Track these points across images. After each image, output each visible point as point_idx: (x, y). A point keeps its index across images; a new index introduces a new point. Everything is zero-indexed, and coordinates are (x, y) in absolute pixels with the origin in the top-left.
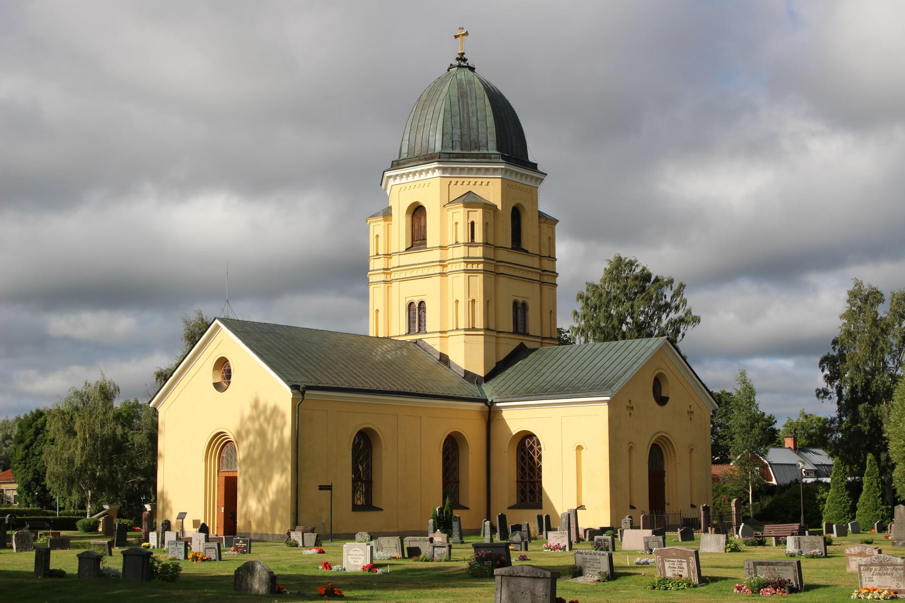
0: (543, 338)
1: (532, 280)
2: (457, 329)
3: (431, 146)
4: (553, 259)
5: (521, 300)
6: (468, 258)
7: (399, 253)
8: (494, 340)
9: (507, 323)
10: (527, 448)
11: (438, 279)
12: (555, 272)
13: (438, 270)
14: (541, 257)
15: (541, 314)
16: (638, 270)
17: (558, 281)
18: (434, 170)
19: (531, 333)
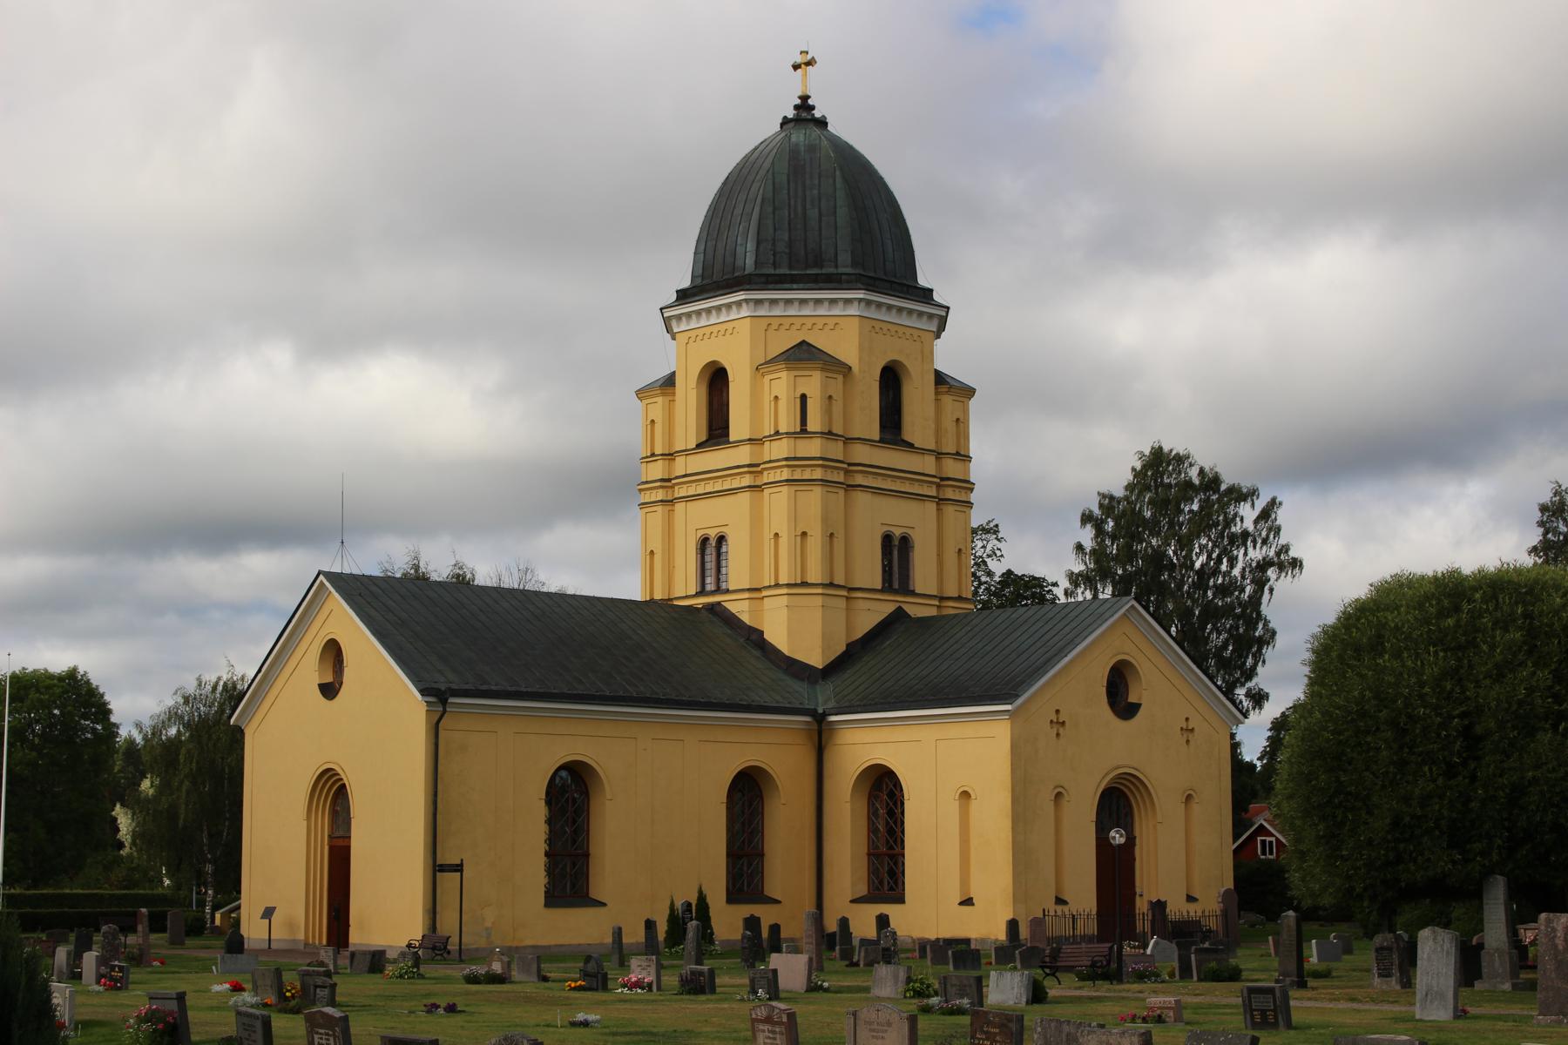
0: (942, 599)
2: (777, 585)
3: (739, 263)
4: (963, 457)
5: (898, 532)
6: (795, 459)
8: (842, 603)
9: (869, 571)
10: (883, 789)
12: (968, 482)
13: (746, 481)
14: (939, 455)
15: (940, 555)
16: (1193, 473)
18: (739, 304)
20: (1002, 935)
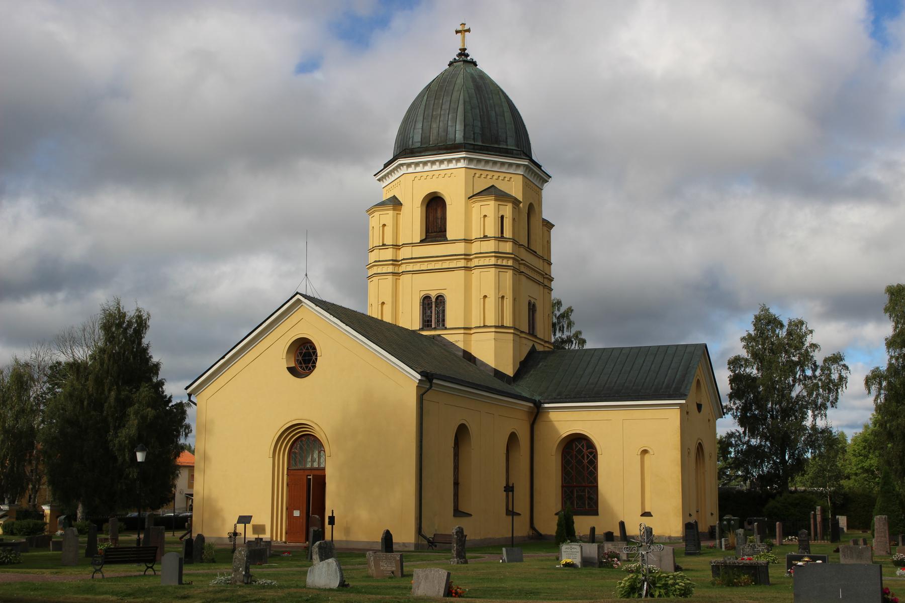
1: (538, 283)
2: (485, 326)
3: (451, 136)
7: (412, 244)
10: (579, 454)
11: (462, 273)
17: (553, 285)
18: (458, 160)
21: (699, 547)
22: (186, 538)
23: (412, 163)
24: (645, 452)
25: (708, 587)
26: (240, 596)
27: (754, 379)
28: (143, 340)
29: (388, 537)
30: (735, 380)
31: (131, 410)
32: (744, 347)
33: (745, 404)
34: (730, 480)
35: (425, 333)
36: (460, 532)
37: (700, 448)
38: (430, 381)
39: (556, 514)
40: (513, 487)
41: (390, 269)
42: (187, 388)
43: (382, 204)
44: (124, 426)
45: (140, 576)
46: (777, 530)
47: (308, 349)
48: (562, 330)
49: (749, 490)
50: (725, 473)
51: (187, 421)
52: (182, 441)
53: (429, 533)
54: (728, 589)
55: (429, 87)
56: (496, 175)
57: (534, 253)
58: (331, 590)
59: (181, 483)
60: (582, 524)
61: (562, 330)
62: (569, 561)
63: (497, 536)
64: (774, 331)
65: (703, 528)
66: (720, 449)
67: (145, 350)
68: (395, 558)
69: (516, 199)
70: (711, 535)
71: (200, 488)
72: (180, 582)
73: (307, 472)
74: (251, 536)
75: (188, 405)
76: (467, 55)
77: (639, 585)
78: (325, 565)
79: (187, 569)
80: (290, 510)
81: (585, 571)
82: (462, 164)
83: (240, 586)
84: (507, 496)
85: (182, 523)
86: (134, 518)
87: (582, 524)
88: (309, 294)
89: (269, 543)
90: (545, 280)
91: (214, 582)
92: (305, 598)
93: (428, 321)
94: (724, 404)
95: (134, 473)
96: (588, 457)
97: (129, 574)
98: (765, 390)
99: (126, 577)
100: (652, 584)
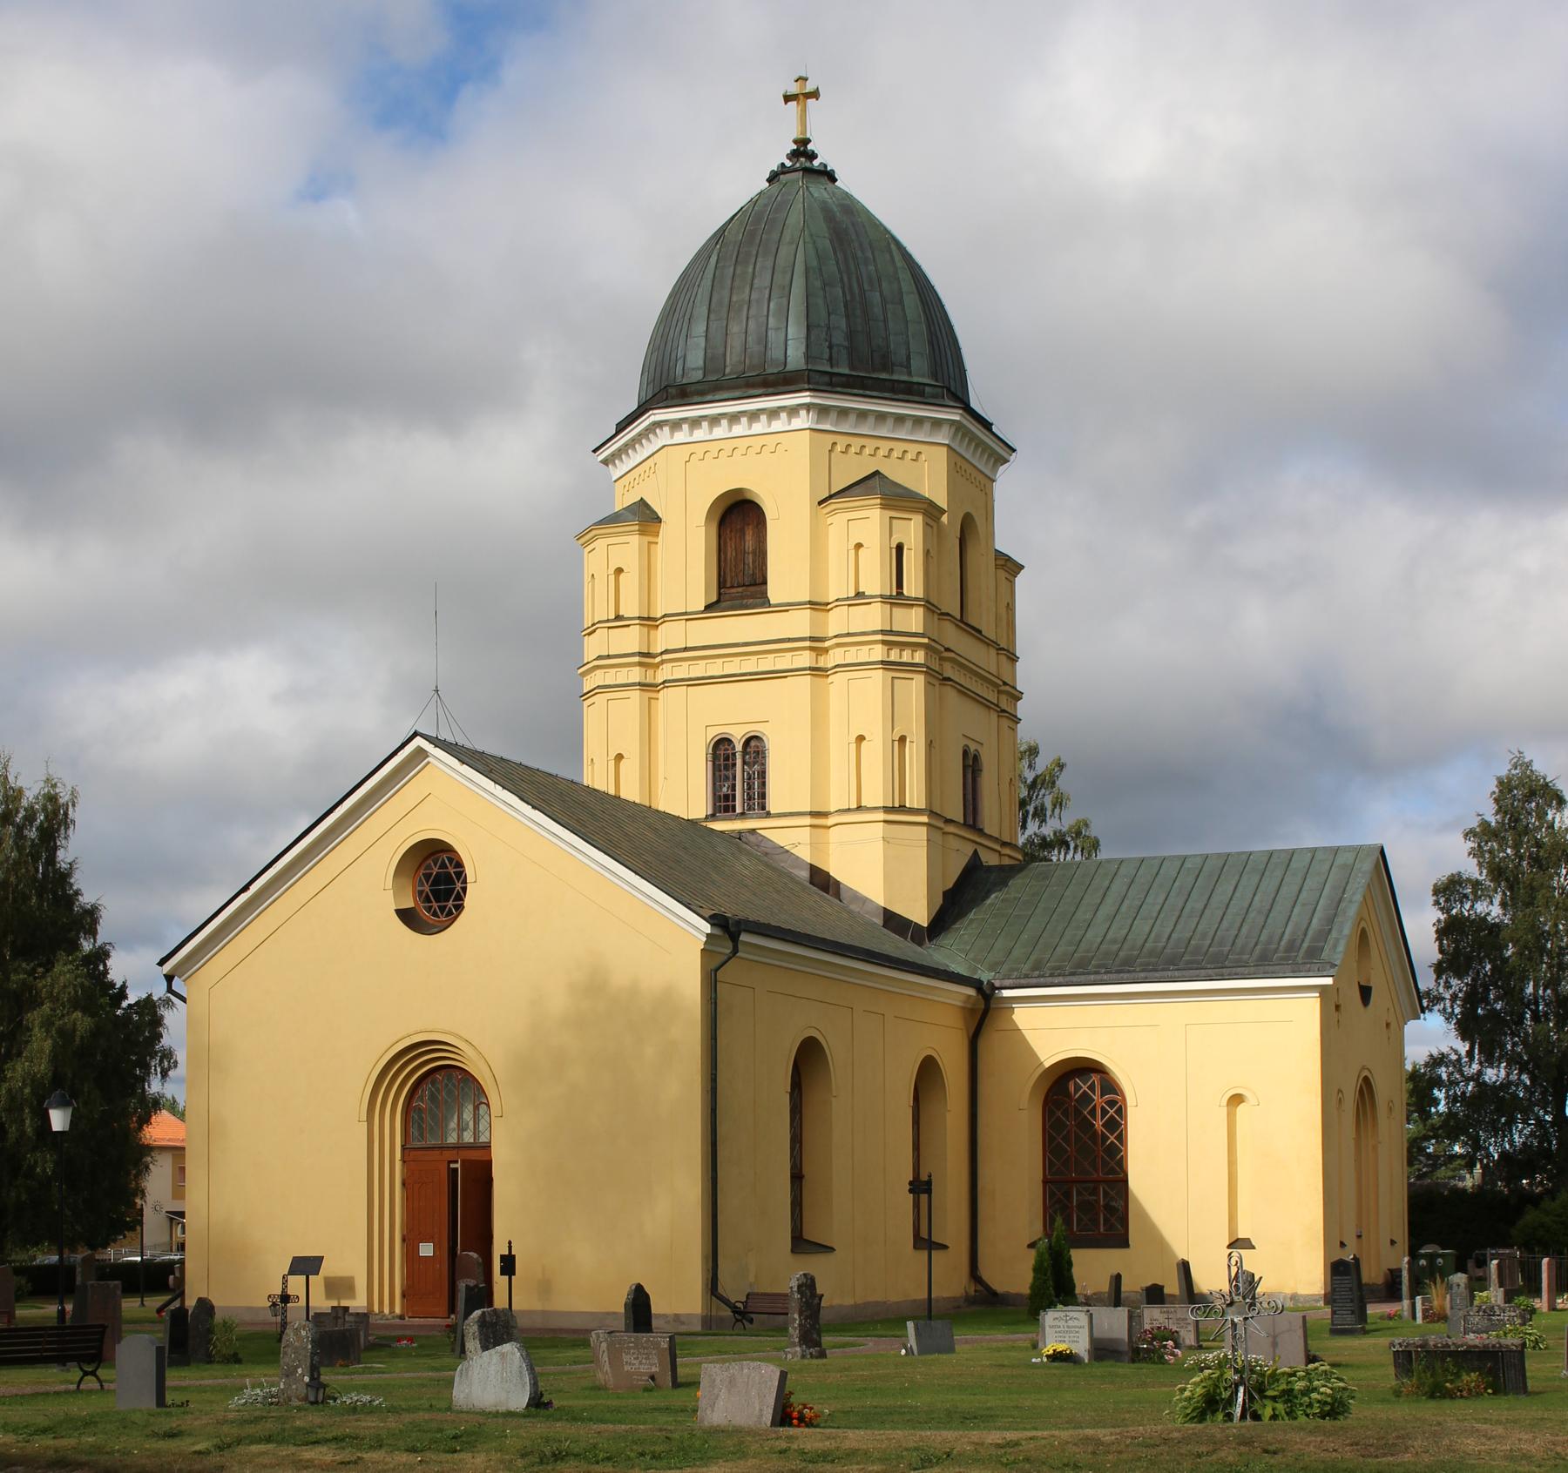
2: (859, 808)
3: (775, 353)
6: (891, 632)
10: (1081, 1110)
11: (806, 681)
13: (805, 659)
17: (1022, 709)
18: (793, 411)
19: (986, 831)
20: (1226, 1288)
21: (1362, 1317)
22: (172, 1307)
23: (684, 420)
24: (1236, 1099)
25: (1383, 1401)
26: (299, 1430)
27: (1495, 928)
28: (60, 854)
29: (639, 1308)
30: (1449, 930)
31: (34, 1018)
32: (1472, 853)
33: (1473, 986)
34: (1435, 1167)
35: (719, 826)
36: (808, 1286)
37: (1366, 1088)
38: (734, 938)
39: (1032, 1245)
40: (929, 1183)
41: (635, 675)
42: (162, 963)
43: (614, 519)
44: (19, 1054)
45: (67, 1392)
46: (1544, 1276)
47: (443, 866)
48: (1040, 814)
49: (1480, 1190)
50: (1422, 1150)
51: (166, 1041)
52: (155, 1086)
53: (735, 1290)
54: (1432, 1404)
55: (721, 232)
56: (885, 447)
57: (976, 632)
58: (510, 1414)
59: (156, 1184)
60: (1091, 1267)
61: (1040, 814)
62: (1061, 1347)
63: (894, 1298)
64: (1542, 815)
65: (1372, 1274)
66: (1411, 1093)
67: (64, 877)
68: (657, 1346)
69: (931, 504)
70: (1391, 1291)
71: (195, 1203)
72: (161, 1401)
73: (448, 1155)
74: (321, 1302)
75: (168, 1003)
76: (813, 156)
77: (1226, 1395)
78: (495, 1359)
79: (174, 1377)
80: (410, 1243)
81: (1102, 1369)
82: (803, 420)
83: (299, 1409)
84: (916, 1205)
85: (159, 1277)
86: (50, 1267)
87: (1091, 1267)
88: (445, 735)
89: (363, 1318)
90: (1001, 699)
91: (238, 1401)
92: (452, 1432)
93: (726, 797)
94: (1423, 987)
95: (45, 1164)
96: (1104, 1112)
97: (43, 1389)
98: (1519, 954)
99: (35, 1395)
100: (1258, 1390)
